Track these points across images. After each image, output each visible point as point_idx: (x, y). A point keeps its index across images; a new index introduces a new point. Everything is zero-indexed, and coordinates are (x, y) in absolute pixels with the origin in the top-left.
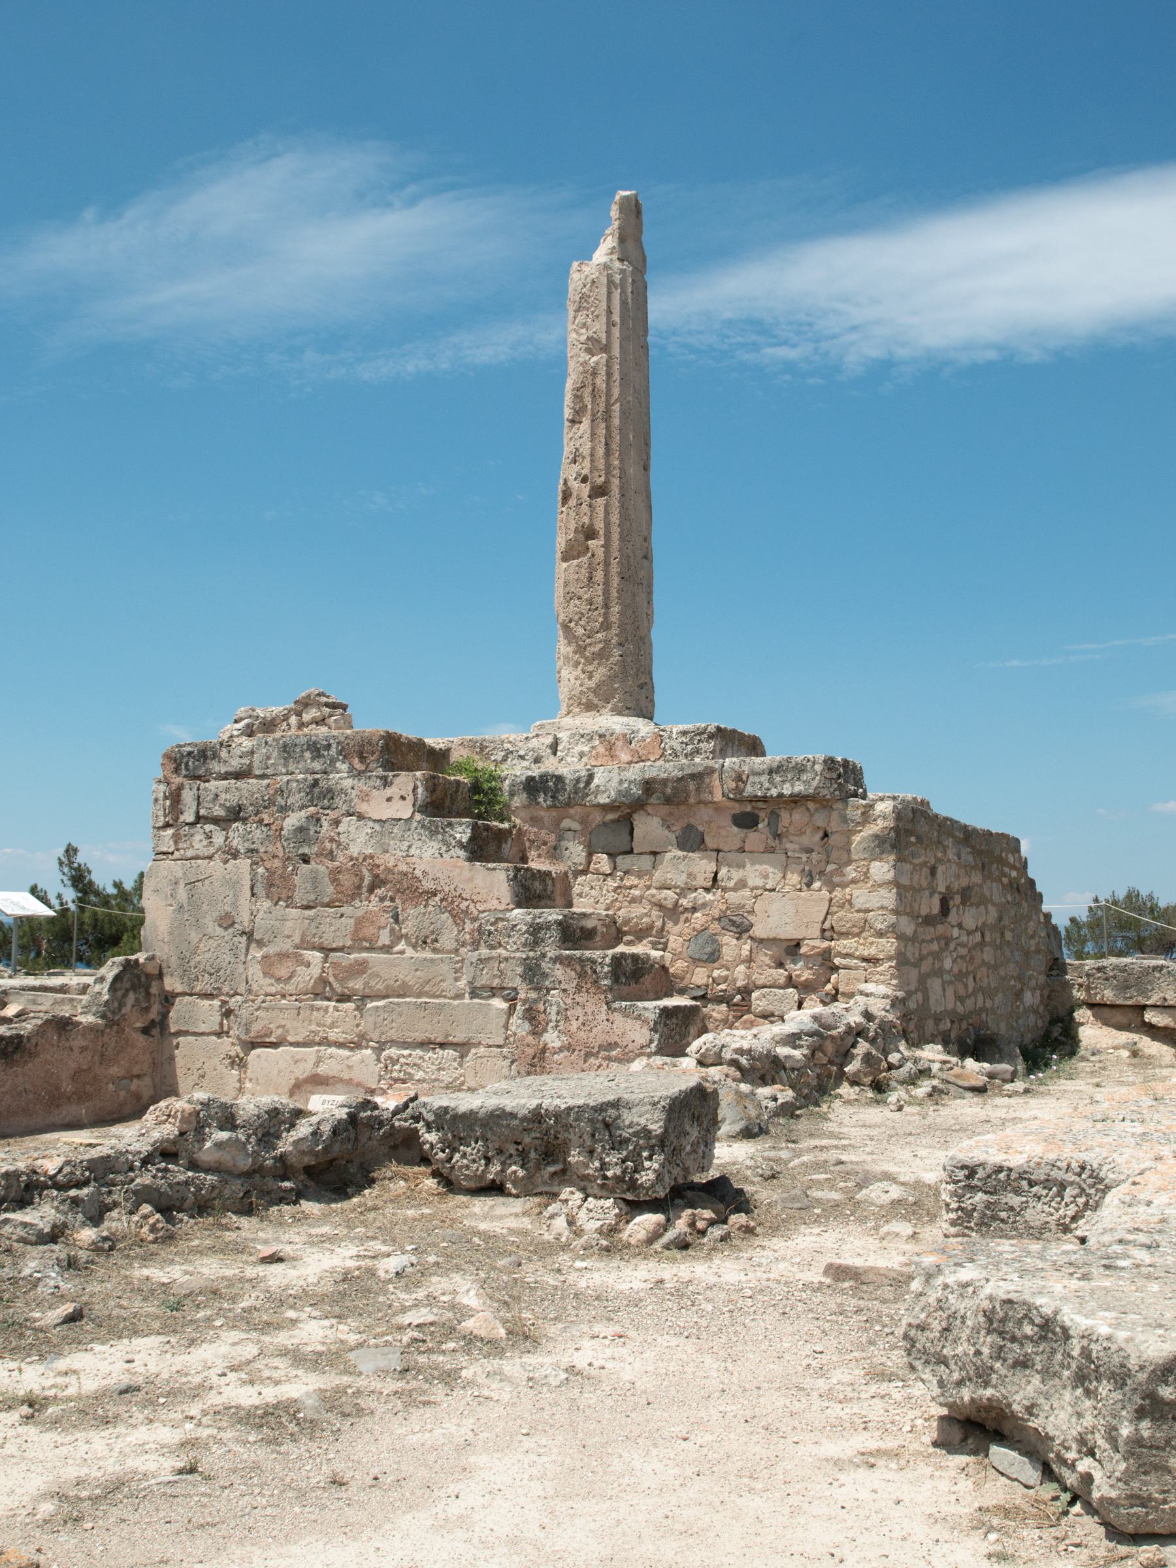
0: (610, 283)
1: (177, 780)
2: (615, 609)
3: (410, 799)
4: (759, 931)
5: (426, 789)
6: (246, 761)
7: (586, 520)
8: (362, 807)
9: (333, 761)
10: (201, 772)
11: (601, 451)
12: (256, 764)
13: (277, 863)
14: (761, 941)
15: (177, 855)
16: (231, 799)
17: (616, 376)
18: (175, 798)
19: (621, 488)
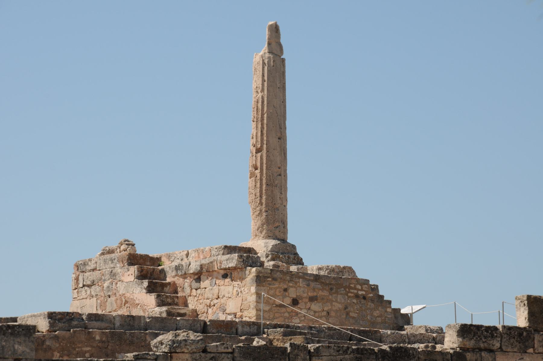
0: (264, 63)
1: (78, 273)
2: (264, 197)
3: (133, 274)
4: (228, 311)
5: (138, 271)
6: (95, 265)
7: (254, 162)
8: (122, 278)
9: (116, 264)
10: (84, 270)
11: (259, 134)
12: (97, 266)
13: (102, 298)
14: (228, 314)
15: (78, 298)
16: (91, 278)
17: (265, 102)
18: (77, 279)
19: (267, 149)
